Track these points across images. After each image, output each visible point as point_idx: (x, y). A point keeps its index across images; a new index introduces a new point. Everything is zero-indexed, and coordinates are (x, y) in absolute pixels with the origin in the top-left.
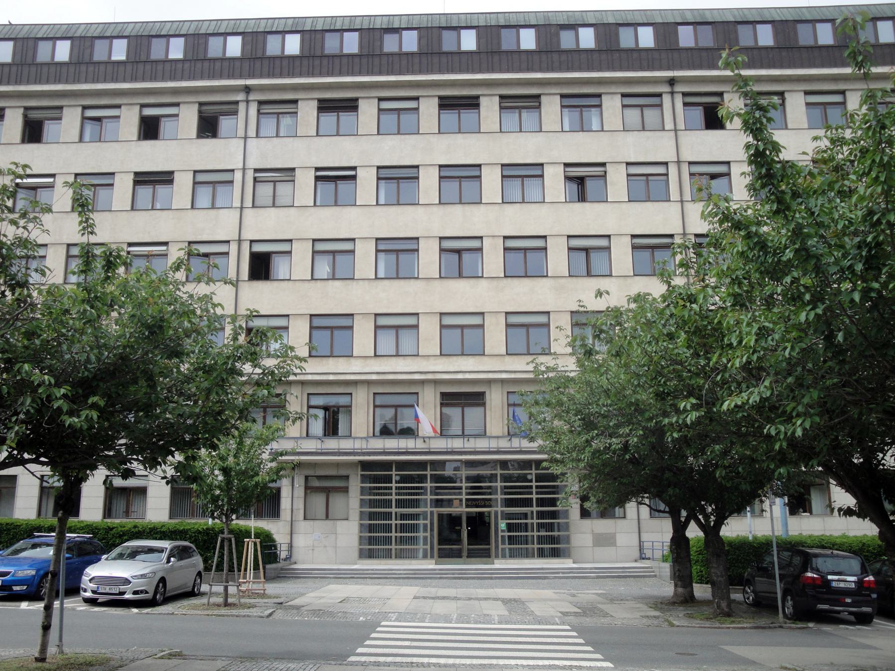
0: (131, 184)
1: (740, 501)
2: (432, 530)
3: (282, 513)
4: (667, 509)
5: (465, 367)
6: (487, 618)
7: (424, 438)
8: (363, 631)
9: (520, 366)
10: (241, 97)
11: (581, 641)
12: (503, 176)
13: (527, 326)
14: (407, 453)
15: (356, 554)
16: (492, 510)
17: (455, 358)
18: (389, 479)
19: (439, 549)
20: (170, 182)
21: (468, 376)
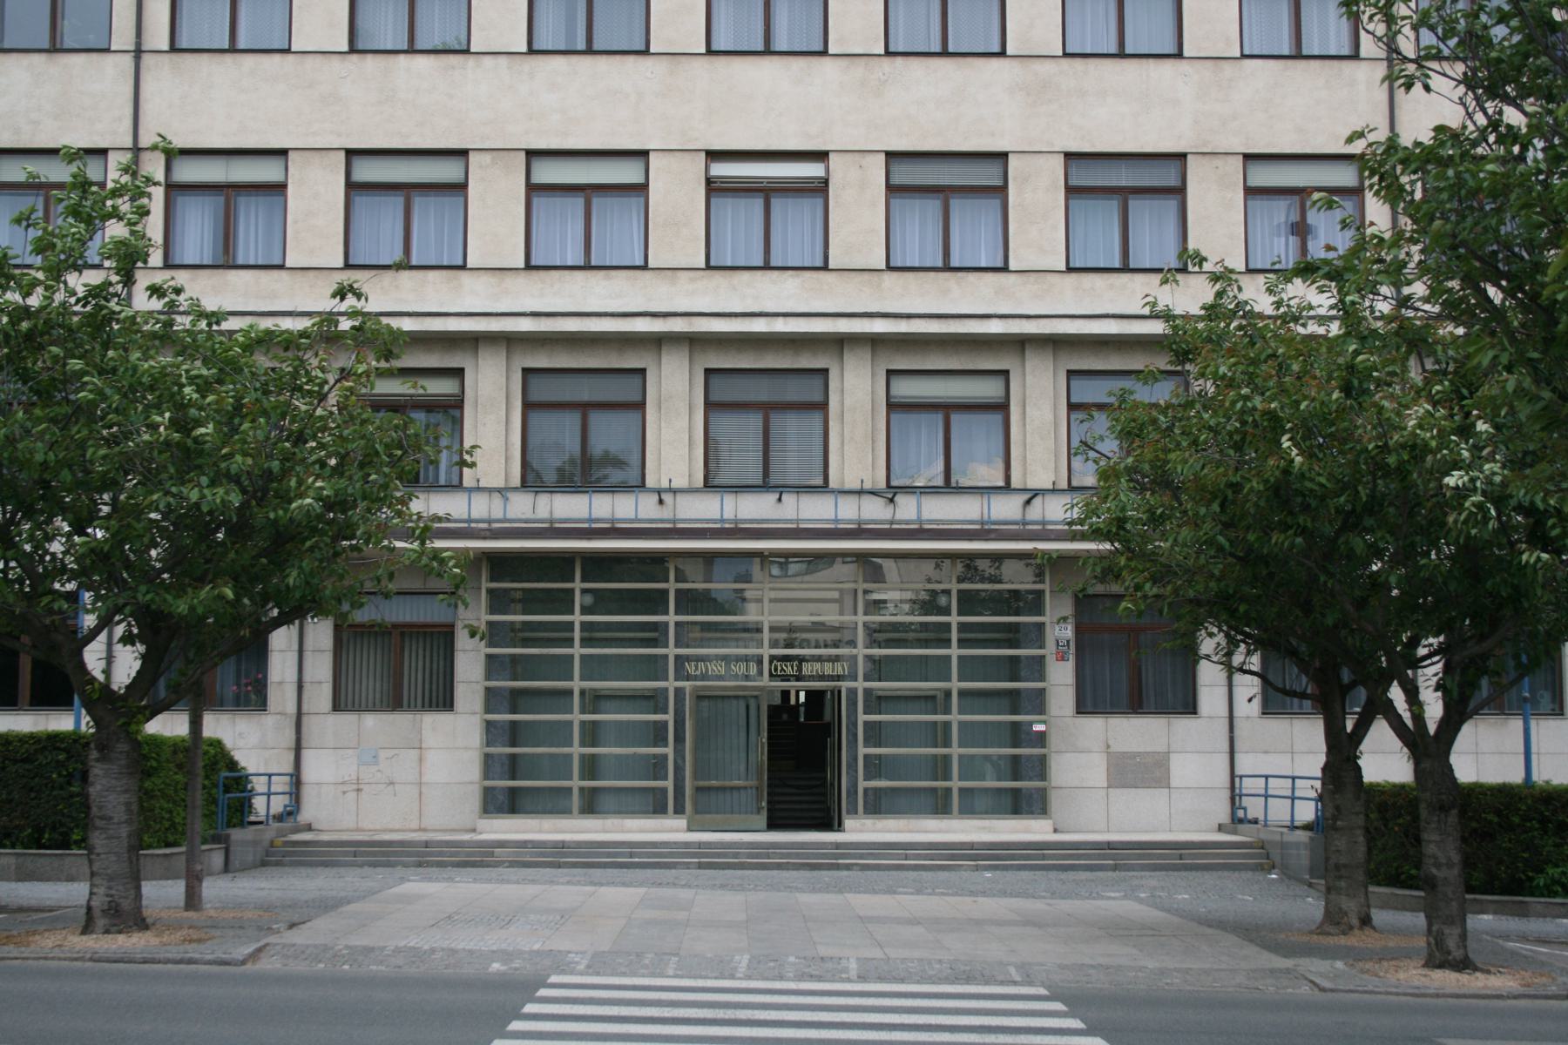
2: (679, 739)
3: (273, 695)
6: (829, 965)
7: (659, 492)
8: (506, 996)
9: (1119, 303)
11: (1076, 1024)
13: (767, 191)
15: (474, 801)
16: (845, 685)
17: (746, 276)
18: (563, 602)
19: (698, 789)
21: (781, 326)
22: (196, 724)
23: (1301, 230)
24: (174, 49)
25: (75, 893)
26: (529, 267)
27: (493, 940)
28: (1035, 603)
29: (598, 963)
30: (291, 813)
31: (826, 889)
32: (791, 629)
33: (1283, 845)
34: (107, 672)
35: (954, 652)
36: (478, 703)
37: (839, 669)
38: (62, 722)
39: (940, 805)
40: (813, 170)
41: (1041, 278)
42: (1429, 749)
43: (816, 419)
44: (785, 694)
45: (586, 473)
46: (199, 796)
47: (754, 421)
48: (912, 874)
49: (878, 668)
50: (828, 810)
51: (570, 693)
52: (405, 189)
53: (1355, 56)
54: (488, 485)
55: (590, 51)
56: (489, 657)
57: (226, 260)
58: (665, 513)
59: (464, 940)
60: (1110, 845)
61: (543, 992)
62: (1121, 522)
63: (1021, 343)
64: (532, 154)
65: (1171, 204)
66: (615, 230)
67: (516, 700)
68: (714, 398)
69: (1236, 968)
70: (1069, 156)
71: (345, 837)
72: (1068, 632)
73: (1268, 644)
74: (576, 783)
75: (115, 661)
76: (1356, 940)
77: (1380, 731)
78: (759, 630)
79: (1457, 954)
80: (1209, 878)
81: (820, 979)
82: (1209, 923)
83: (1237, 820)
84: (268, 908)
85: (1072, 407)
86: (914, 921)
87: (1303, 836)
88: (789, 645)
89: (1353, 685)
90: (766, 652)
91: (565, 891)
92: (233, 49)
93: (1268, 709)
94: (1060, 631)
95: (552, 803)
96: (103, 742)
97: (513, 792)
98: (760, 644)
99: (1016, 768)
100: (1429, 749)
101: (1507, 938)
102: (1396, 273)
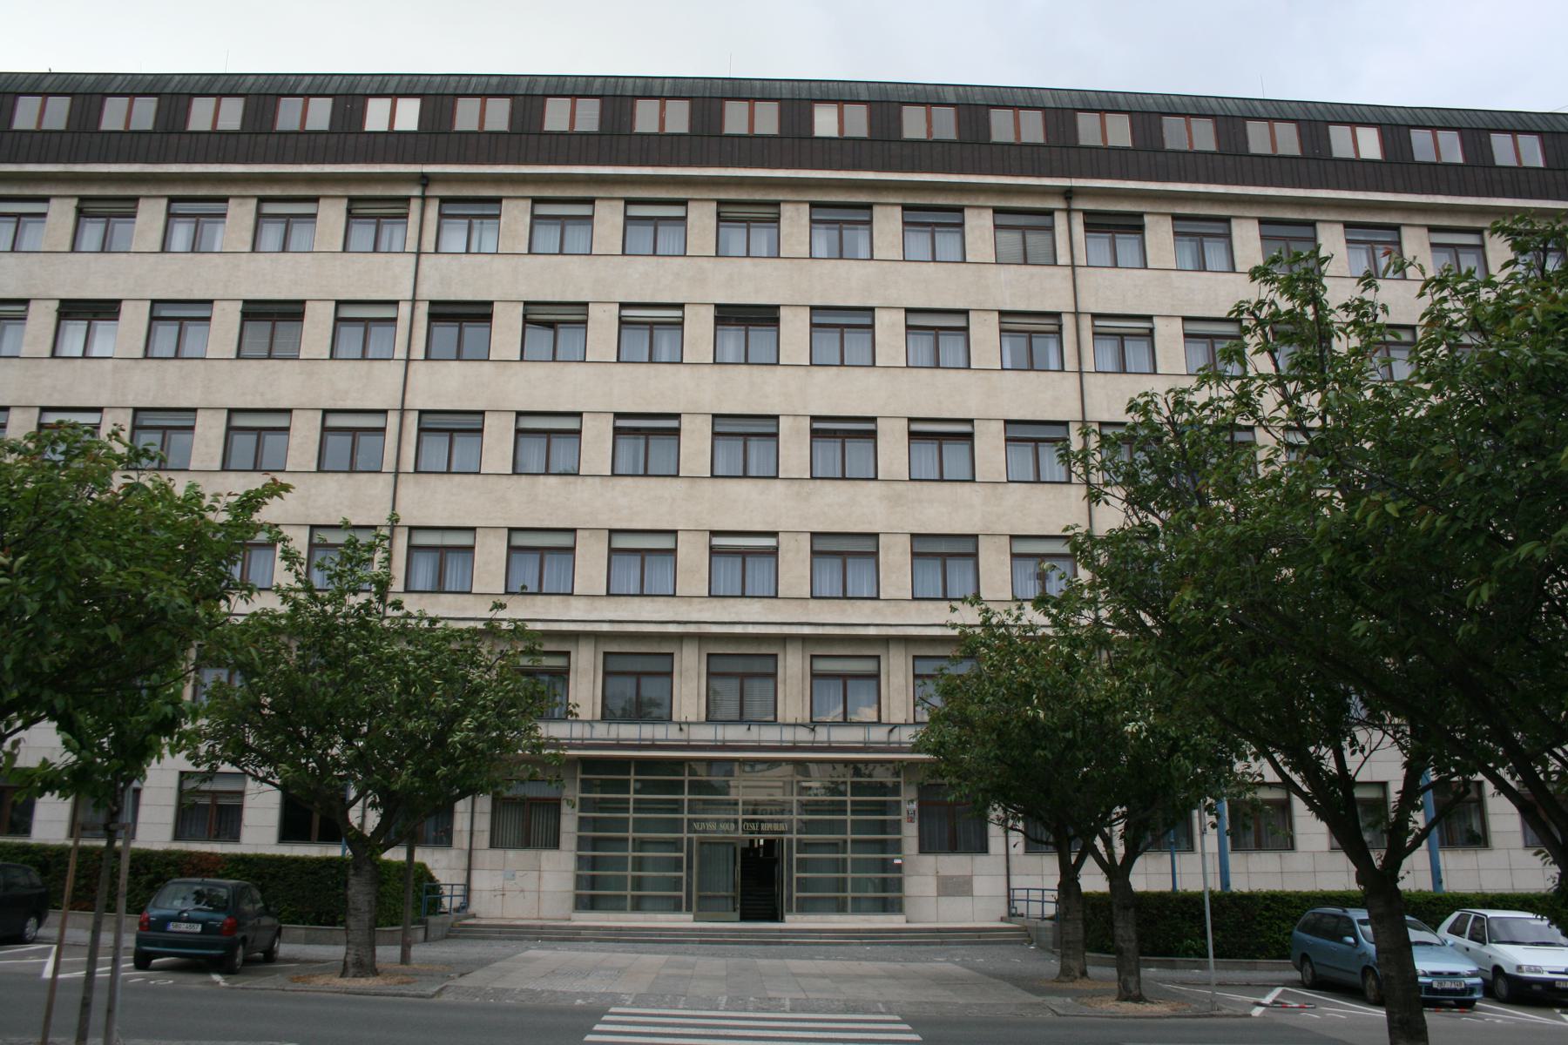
0: (237, 317)
1: (1161, 826)
2: (690, 867)
4: (1051, 839)
5: (749, 615)
9: (934, 618)
10: (417, 192)
12: (812, 325)
13: (744, 553)
14: (653, 746)
15: (570, 902)
16: (786, 836)
17: (732, 601)
18: (623, 786)
19: (700, 897)
20: (488, 318)
21: (751, 630)
22: (410, 854)
23: (1042, 577)
24: (416, 471)
25: (337, 952)
26: (609, 594)
27: (577, 986)
28: (896, 790)
29: (639, 1000)
30: (464, 907)
31: (773, 957)
32: (756, 803)
33: (1038, 929)
34: (362, 825)
35: (849, 817)
36: (574, 846)
37: (782, 827)
38: (335, 851)
39: (840, 907)
40: (770, 542)
41: (898, 604)
42: (1117, 873)
43: (770, 683)
44: (752, 841)
45: (640, 712)
46: (411, 897)
47: (734, 684)
48: (824, 948)
49: (807, 827)
50: (776, 909)
51: (626, 839)
52: (541, 552)
53: (1069, 482)
54: (583, 717)
55: (646, 475)
56: (581, 818)
57: (439, 589)
58: (683, 736)
59: (562, 985)
60: (939, 930)
61: (606, 1018)
62: (942, 744)
63: (886, 640)
64: (612, 532)
65: (971, 562)
66: (658, 575)
67: (595, 843)
68: (713, 670)
69: (1007, 1002)
70: (913, 535)
71: (495, 922)
72: (914, 806)
73: (1029, 815)
74: (629, 893)
75: (365, 817)
76: (1079, 985)
77: (1090, 864)
78: (736, 803)
79: (1136, 992)
80: (995, 949)
81: (768, 1011)
82: (995, 976)
83: (1011, 915)
84: (449, 964)
85: (916, 676)
86: (823, 976)
87: (1048, 924)
88: (755, 813)
89: (1074, 837)
90: (740, 817)
91: (621, 957)
92: (449, 472)
93: (1029, 850)
94: (909, 803)
95: (616, 905)
96: (357, 864)
97: (593, 897)
98: (736, 812)
99: (884, 885)
100: (1117, 873)
101: (1164, 981)
102: (1092, 602)
